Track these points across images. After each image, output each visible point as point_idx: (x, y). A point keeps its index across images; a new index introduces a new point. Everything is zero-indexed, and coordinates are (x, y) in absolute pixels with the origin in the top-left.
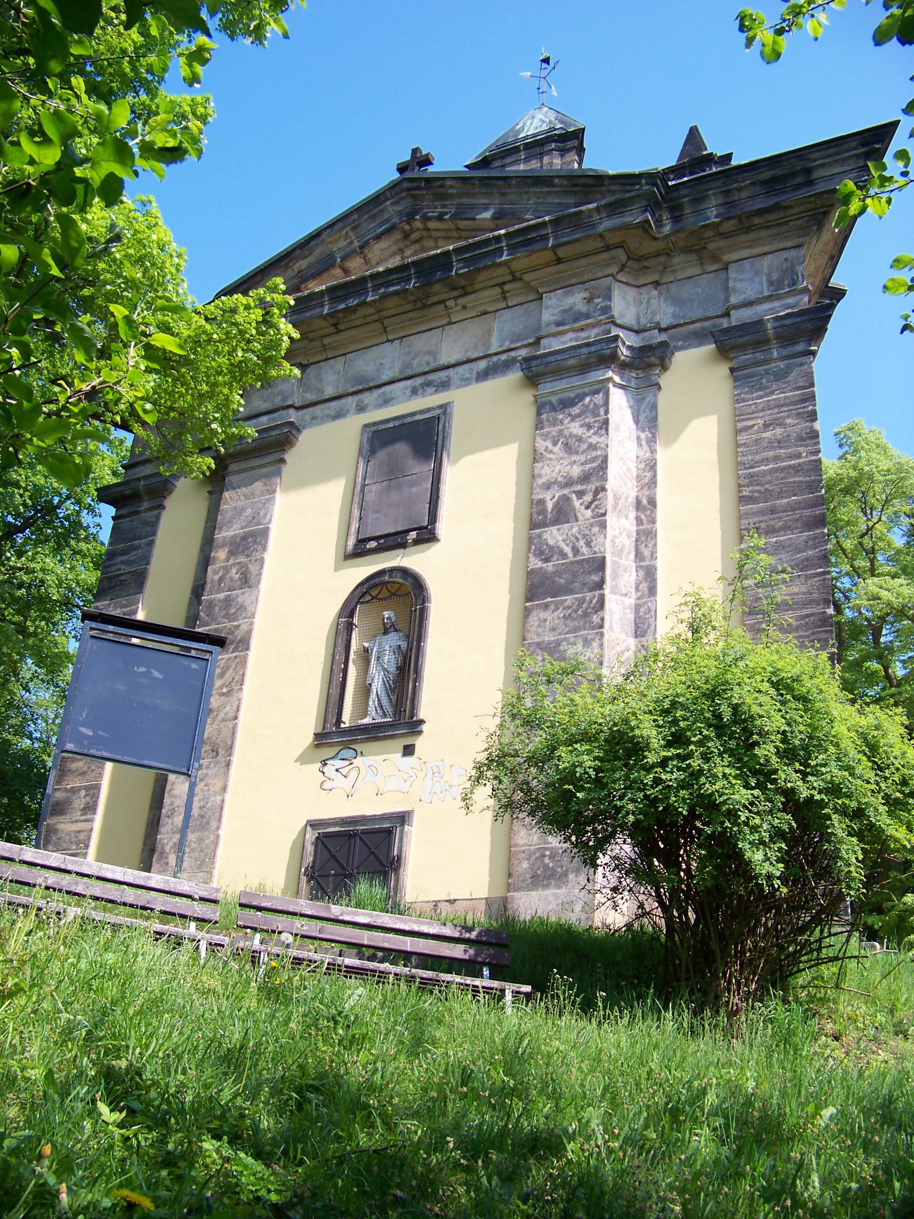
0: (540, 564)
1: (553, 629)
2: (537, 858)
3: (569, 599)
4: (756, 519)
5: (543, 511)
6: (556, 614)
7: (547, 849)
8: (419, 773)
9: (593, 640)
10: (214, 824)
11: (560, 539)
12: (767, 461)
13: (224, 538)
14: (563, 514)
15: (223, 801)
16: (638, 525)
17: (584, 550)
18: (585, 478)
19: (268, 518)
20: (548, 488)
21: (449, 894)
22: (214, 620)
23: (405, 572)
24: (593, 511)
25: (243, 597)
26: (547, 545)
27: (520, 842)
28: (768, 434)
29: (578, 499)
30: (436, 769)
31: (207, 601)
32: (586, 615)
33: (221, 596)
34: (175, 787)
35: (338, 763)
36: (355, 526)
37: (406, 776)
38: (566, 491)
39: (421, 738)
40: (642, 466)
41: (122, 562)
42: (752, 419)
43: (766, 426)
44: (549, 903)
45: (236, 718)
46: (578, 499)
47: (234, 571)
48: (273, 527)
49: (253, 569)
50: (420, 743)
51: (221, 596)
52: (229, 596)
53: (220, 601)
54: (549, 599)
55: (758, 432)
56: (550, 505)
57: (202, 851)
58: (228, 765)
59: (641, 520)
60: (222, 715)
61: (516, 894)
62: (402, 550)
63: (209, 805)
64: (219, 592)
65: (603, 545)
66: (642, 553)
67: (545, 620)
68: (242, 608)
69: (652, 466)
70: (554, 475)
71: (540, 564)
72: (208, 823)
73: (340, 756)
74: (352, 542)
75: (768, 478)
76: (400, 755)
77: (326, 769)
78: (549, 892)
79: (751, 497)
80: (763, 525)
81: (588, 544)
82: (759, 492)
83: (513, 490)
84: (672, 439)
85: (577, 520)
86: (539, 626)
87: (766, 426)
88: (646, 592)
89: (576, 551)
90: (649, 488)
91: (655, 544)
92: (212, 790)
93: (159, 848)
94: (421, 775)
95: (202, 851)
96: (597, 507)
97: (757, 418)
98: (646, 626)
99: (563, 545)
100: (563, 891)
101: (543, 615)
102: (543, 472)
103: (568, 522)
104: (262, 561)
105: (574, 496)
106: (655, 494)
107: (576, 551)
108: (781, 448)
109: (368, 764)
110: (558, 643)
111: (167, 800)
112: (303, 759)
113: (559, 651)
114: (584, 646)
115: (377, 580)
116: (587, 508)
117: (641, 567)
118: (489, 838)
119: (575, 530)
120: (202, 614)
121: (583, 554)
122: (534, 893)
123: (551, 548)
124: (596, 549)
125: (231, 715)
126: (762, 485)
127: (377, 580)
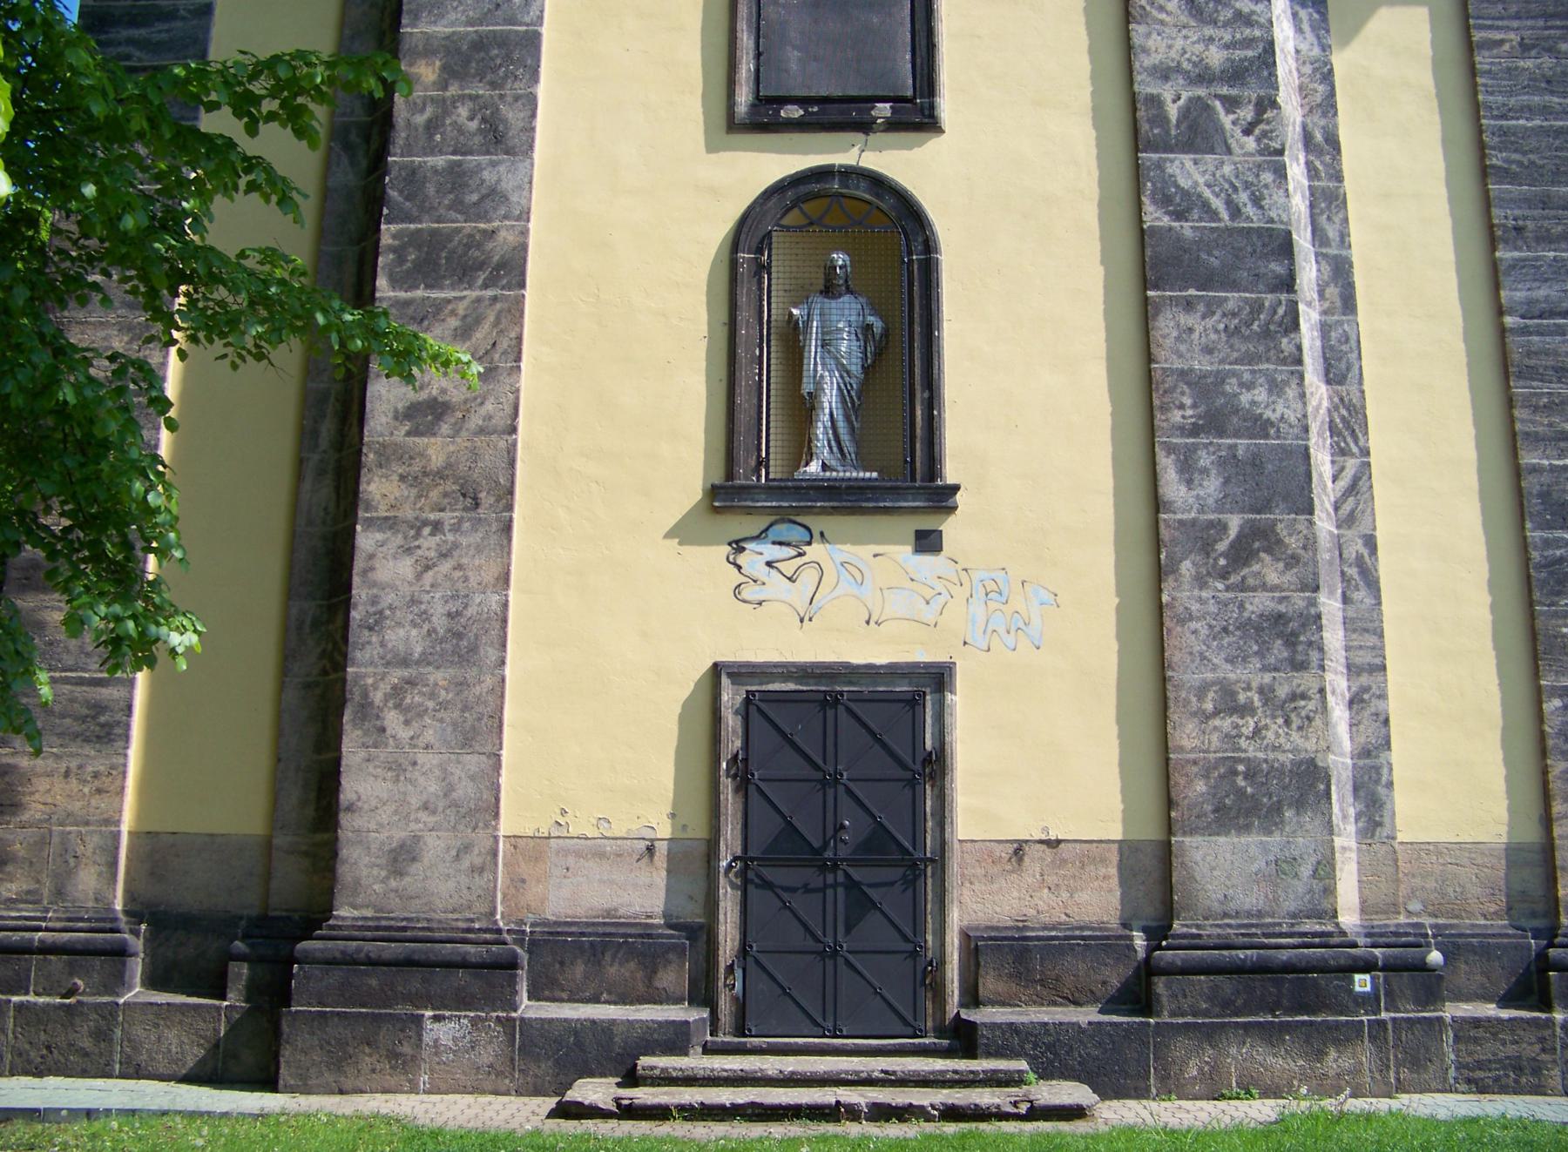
0: (1166, 221)
1: (1208, 350)
2: (1221, 777)
3: (1233, 299)
4: (1517, 212)
5: (1161, 119)
6: (1210, 322)
7: (1240, 760)
8: (955, 590)
9: (1286, 383)
10: (492, 654)
11: (1201, 180)
12: (1529, 111)
13: (428, 37)
14: (1198, 134)
15: (505, 605)
16: (1310, 178)
17: (1250, 210)
18: (1235, 74)
19: (534, 12)
20: (1166, 78)
21: (1046, 830)
22: (426, 209)
23: (878, 182)
24: (1258, 140)
25: (493, 171)
26: (1177, 186)
27: (1187, 743)
28: (1529, 64)
29: (1228, 112)
30: (991, 586)
31: (403, 167)
32: (1266, 334)
33: (440, 161)
34: (377, 563)
35: (771, 551)
36: (746, 67)
37: (928, 593)
38: (1201, 92)
39: (952, 519)
40: (1308, 69)
41: (131, 42)
42: (1498, 28)
43: (1525, 48)
44: (1253, 859)
45: (513, 430)
46: (1228, 112)
47: (463, 112)
48: (546, 31)
49: (512, 115)
50: (951, 529)
51: (440, 161)
52: (459, 164)
53: (435, 171)
54: (1192, 292)
55: (1510, 55)
56: (1173, 111)
57: (465, 708)
58: (507, 528)
59: (1316, 169)
60: (475, 421)
61: (1187, 840)
62: (861, 136)
63: (471, 611)
64: (432, 150)
65: (1287, 209)
66: (1323, 230)
67: (1191, 330)
68: (494, 195)
69: (1328, 77)
70: (1173, 54)
71: (1166, 221)
72: (474, 649)
73: (772, 535)
74: (744, 97)
75: (1534, 143)
76: (909, 549)
77: (742, 559)
78: (1252, 840)
79: (1506, 171)
80: (1530, 224)
81: (1257, 201)
82: (1520, 164)
83: (1083, 64)
84: (1346, 41)
85: (1229, 151)
86: (1178, 339)
87: (1525, 48)
88: (1338, 304)
89: (1235, 212)
90: (1324, 115)
91: (1346, 220)
92: (473, 582)
93: (355, 695)
94: (961, 593)
95: (465, 708)
96: (1265, 134)
97: (1508, 29)
98: (1343, 366)
99: (1207, 193)
100: (1276, 839)
101: (1186, 320)
102: (1151, 43)
103: (1212, 151)
104: (532, 101)
105: (1218, 103)
106: (1336, 126)
107: (1235, 212)
108: (1552, 93)
109: (839, 558)
110: (1221, 378)
111: (360, 592)
112: (683, 532)
113: (1224, 394)
114: (1270, 391)
115: (816, 187)
116: (1247, 132)
117: (1325, 256)
118: (1114, 730)
119: (1227, 169)
120: (393, 194)
121: (1248, 218)
122: (1222, 839)
123: (1185, 194)
124: (1273, 214)
125: (500, 421)
126: (1524, 153)
127: (816, 187)
